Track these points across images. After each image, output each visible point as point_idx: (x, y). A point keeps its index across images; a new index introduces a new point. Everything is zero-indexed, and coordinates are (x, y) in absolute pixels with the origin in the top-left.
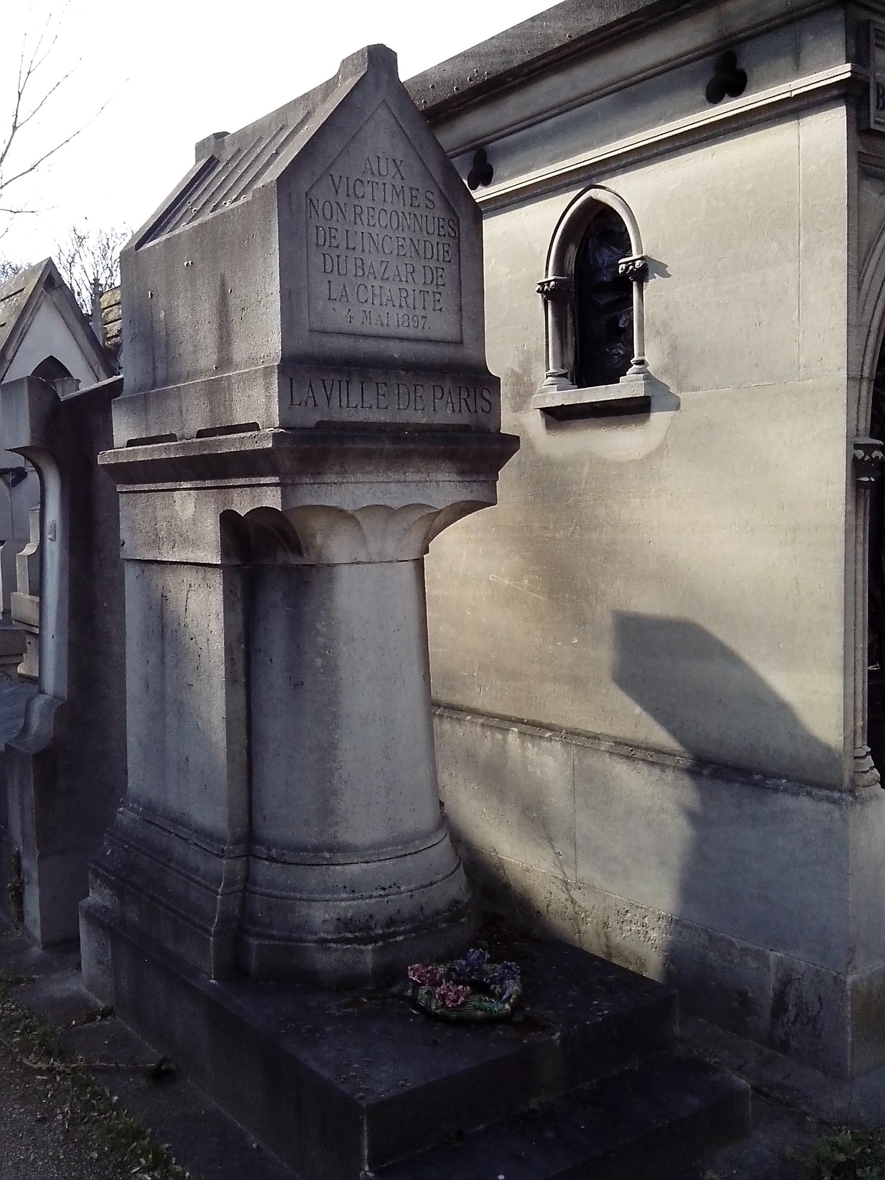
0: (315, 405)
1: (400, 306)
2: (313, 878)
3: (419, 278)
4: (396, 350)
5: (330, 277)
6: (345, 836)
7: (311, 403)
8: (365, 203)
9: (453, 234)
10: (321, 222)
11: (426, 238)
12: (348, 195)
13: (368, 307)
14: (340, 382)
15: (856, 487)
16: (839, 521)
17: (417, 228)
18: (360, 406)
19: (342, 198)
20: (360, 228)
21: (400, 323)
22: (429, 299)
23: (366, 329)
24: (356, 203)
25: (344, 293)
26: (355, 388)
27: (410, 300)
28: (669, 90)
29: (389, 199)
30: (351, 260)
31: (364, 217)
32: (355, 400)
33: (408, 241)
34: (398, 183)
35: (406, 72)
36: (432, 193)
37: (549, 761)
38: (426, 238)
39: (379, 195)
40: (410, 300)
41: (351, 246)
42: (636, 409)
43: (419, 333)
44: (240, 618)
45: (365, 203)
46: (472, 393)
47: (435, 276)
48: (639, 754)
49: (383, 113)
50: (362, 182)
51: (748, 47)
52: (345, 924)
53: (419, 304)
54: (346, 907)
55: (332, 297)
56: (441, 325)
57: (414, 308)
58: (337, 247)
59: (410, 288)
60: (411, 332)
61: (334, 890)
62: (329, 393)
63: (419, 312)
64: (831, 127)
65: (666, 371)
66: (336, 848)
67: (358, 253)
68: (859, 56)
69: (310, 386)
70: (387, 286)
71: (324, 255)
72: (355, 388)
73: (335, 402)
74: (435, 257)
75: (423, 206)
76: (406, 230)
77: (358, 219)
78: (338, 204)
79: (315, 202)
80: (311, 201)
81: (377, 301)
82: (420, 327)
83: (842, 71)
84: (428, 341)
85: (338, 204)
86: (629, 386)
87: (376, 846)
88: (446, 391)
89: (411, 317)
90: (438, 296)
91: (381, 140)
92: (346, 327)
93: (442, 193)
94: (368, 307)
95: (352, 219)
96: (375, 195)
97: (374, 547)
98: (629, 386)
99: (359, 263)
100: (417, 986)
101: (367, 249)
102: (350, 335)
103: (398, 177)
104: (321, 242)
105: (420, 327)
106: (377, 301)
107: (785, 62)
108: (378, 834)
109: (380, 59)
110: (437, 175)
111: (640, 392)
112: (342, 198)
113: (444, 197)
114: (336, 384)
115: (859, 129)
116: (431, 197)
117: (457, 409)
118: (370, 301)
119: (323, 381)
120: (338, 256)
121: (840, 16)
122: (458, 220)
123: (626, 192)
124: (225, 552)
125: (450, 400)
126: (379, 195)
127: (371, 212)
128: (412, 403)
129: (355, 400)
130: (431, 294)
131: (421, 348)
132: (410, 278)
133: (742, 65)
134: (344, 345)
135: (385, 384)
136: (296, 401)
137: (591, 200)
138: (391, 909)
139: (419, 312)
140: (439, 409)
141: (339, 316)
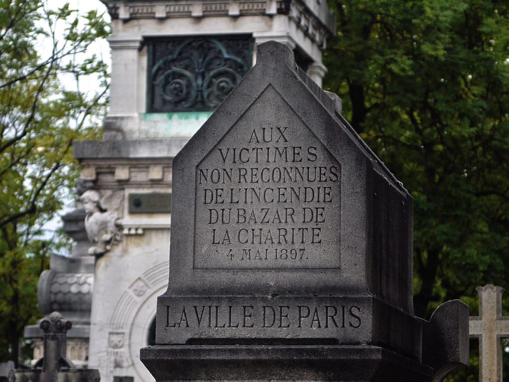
0: (188, 326)
1: (279, 242)
4: (271, 279)
5: (216, 227)
7: (184, 323)
9: (334, 178)
10: (209, 185)
11: (307, 184)
12: (234, 162)
13: (248, 246)
14: (210, 307)
17: (298, 178)
18: (227, 325)
19: (228, 165)
20: (244, 185)
21: (278, 256)
22: (308, 235)
24: (241, 166)
25: (227, 238)
26: (224, 308)
27: (289, 237)
29: (271, 159)
30: (234, 210)
31: (248, 177)
32: (223, 320)
33: (289, 190)
34: (281, 145)
36: (315, 149)
38: (307, 184)
39: (262, 158)
40: (289, 237)
41: (235, 199)
44: (151, 56)
46: (340, 313)
47: (315, 215)
50: (248, 150)
53: (298, 239)
55: (215, 242)
57: (293, 243)
58: (223, 202)
59: (289, 227)
62: (199, 316)
63: (297, 246)
67: (240, 206)
69: (184, 311)
70: (265, 228)
71: (211, 210)
72: (224, 308)
73: (205, 323)
74: (316, 199)
75: (305, 160)
76: (287, 181)
77: (242, 180)
78: (225, 170)
79: (205, 171)
80: (201, 170)
81: (256, 240)
82: (298, 258)
84: (306, 269)
85: (225, 170)
88: (312, 311)
89: (289, 251)
90: (316, 232)
93: (323, 145)
94: (248, 246)
95: (237, 180)
96: (259, 159)
99: (241, 212)
101: (249, 200)
102: (228, 269)
103: (282, 139)
104: (208, 200)
105: (298, 258)
106: (256, 240)
110: (320, 133)
112: (228, 165)
113: (327, 150)
114: (207, 310)
116: (313, 151)
117: (323, 324)
118: (250, 241)
119: (195, 307)
120: (223, 210)
122: (340, 165)
125: (316, 318)
126: (262, 158)
127: (255, 172)
128: (277, 322)
129: (223, 320)
130: (310, 230)
132: (289, 220)
134: (224, 278)
135: (252, 307)
136: (171, 322)
139: (297, 246)
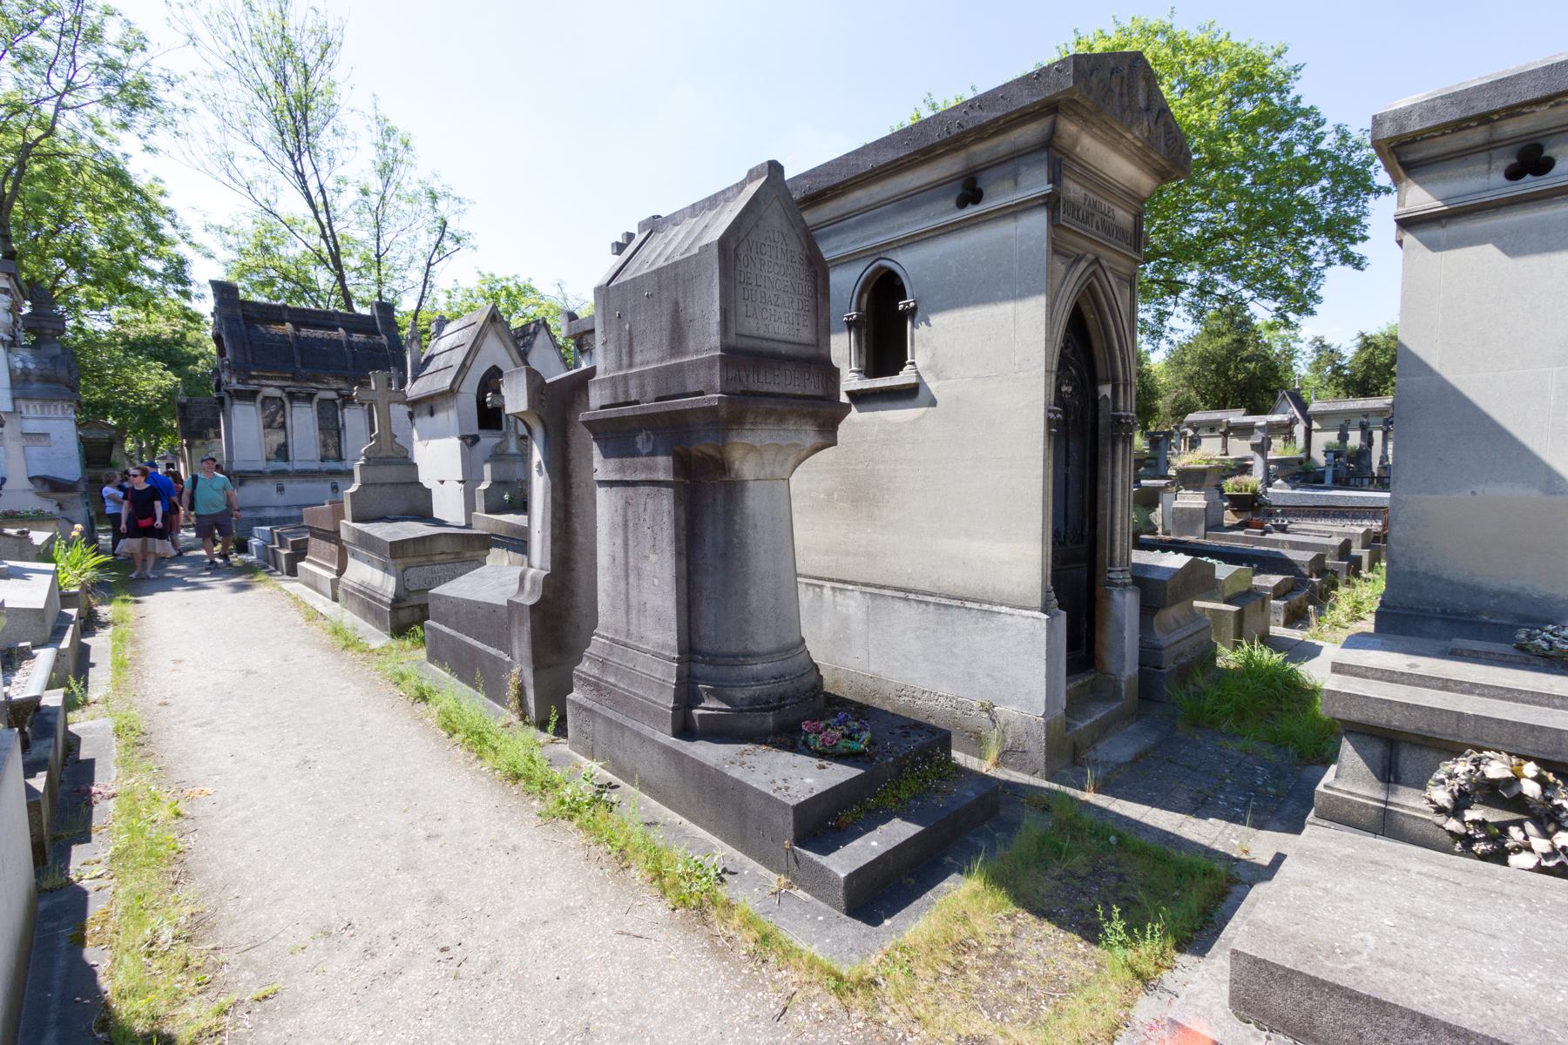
2: (734, 673)
3: (795, 305)
4: (783, 349)
6: (752, 647)
8: (766, 258)
15: (1049, 434)
16: (1040, 454)
23: (767, 335)
28: (931, 200)
35: (788, 175)
37: (852, 602)
42: (908, 394)
43: (795, 339)
45: (766, 258)
48: (912, 596)
49: (776, 204)
51: (984, 175)
52: (754, 700)
54: (754, 690)
56: (806, 335)
60: (791, 338)
61: (747, 680)
64: (1038, 222)
65: (929, 368)
66: (747, 655)
68: (1055, 179)
83: (1047, 188)
86: (905, 377)
87: (771, 653)
91: (775, 221)
92: (755, 333)
97: (768, 470)
98: (905, 377)
100: (807, 734)
107: (1008, 184)
108: (772, 646)
109: (775, 168)
111: (913, 380)
112: (753, 254)
115: (1054, 223)
121: (1044, 155)
123: (907, 263)
124: (676, 474)
129: (762, 379)
131: (795, 348)
133: (979, 185)
137: (881, 268)
138: (781, 690)
140: (812, 387)
141: (753, 326)
